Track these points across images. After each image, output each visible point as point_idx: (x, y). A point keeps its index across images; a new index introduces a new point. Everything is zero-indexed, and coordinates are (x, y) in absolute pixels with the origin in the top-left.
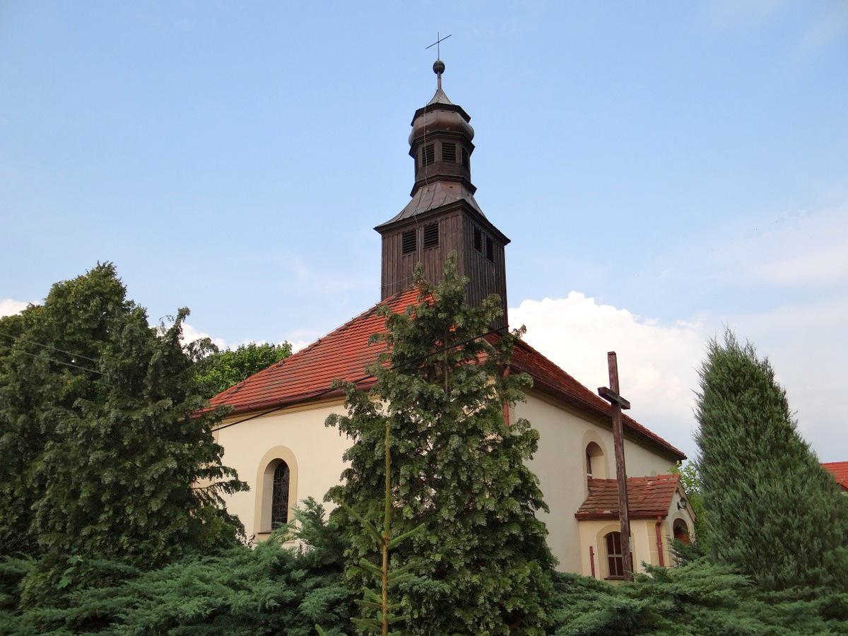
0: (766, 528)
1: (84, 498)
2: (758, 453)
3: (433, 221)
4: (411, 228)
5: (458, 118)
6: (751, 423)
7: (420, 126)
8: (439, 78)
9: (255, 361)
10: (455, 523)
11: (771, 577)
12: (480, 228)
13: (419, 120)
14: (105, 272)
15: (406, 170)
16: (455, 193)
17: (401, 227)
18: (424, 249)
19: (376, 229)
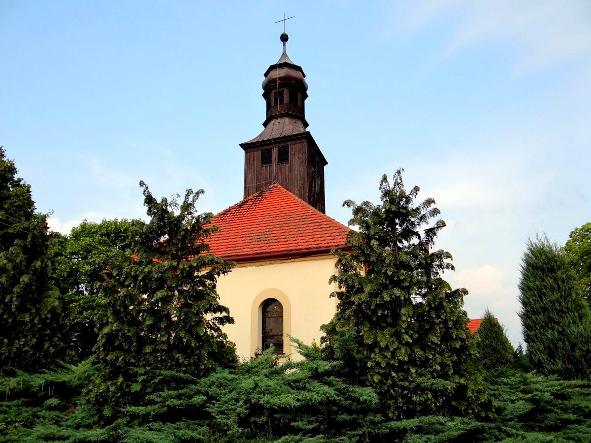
0: (577, 353)
1: (148, 325)
2: (567, 308)
6: (563, 291)
7: (274, 77)
8: (284, 45)
9: (119, 233)
10: (441, 344)
14: (327, 163)
15: (260, 107)
17: (263, 145)
19: (242, 145)
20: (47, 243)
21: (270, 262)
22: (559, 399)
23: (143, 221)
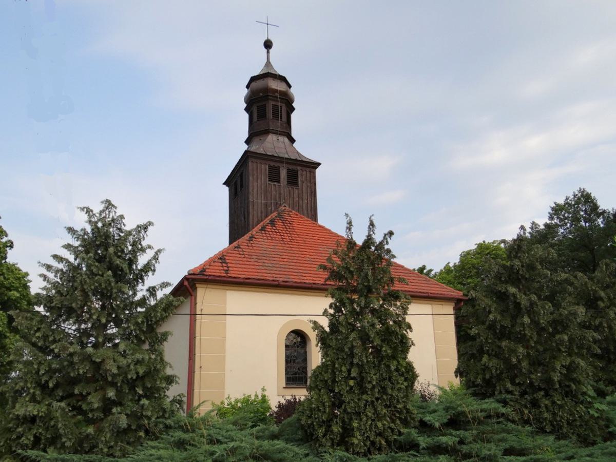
8: (268, 52)
12: (294, 167)
13: (253, 84)
20: (59, 280)
23: (476, 246)
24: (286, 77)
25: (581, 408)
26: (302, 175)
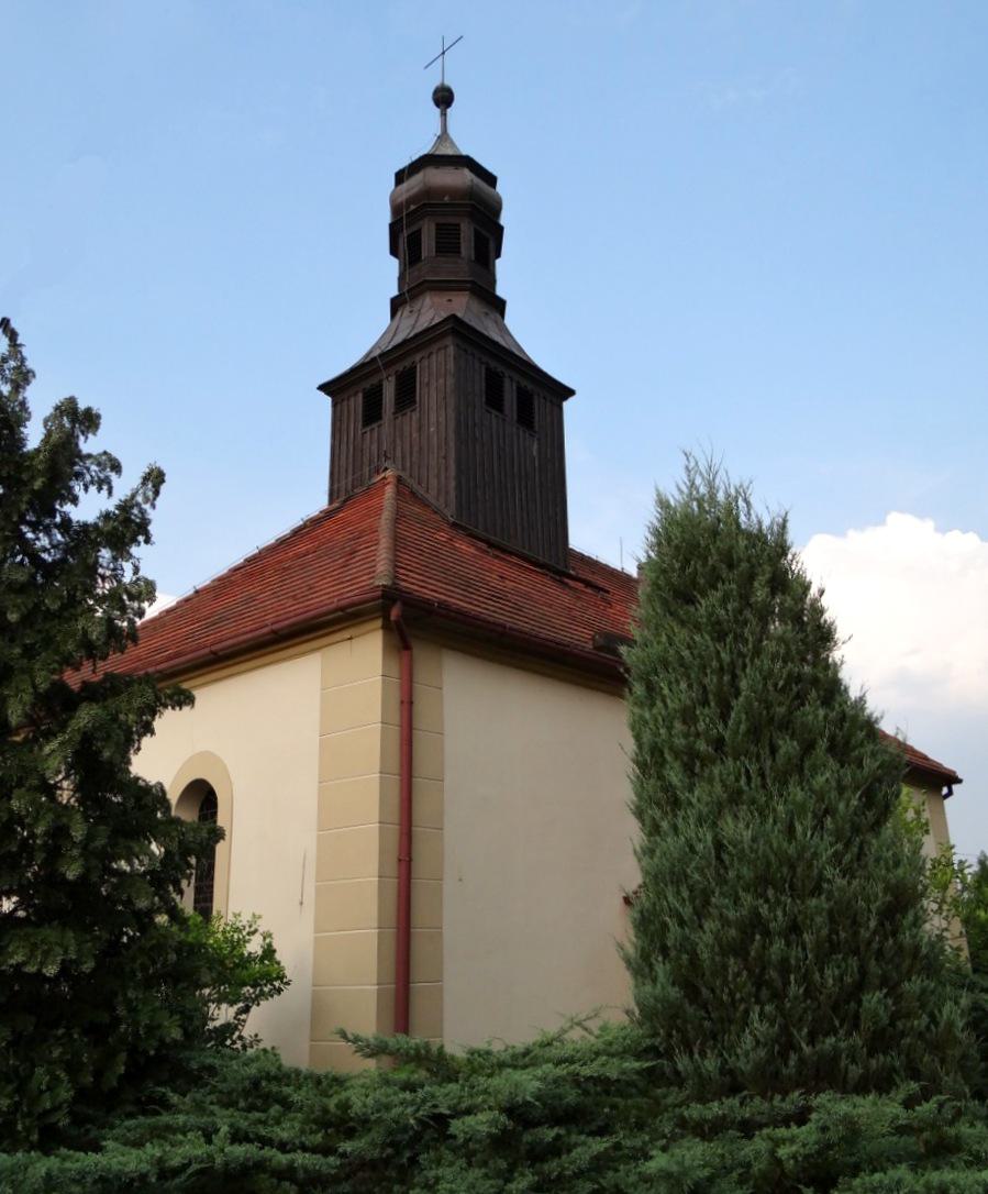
3: (407, 363)
4: (374, 381)
5: (465, 177)
8: (444, 114)
11: (710, 1064)
12: (500, 369)
16: (461, 305)
18: (394, 414)
19: (322, 388)
21: (346, 634)
22: (50, 564)
24: (472, 156)
25: (706, 641)
26: (539, 405)
